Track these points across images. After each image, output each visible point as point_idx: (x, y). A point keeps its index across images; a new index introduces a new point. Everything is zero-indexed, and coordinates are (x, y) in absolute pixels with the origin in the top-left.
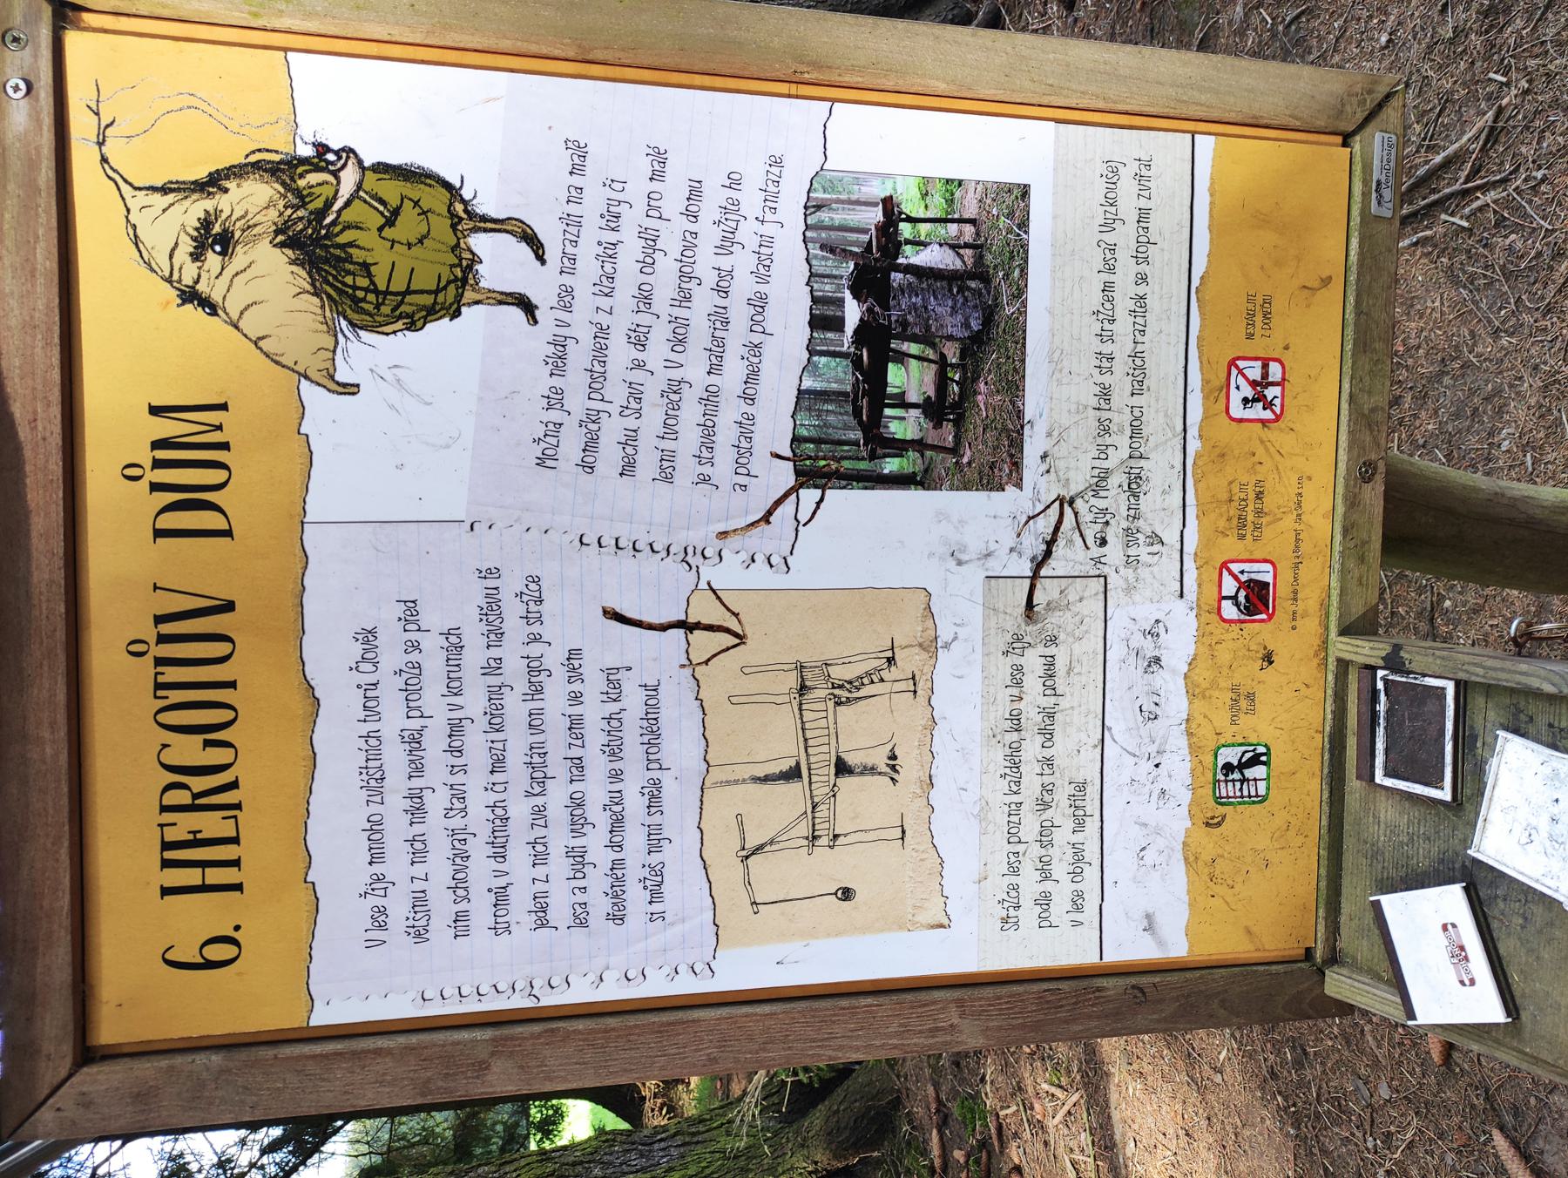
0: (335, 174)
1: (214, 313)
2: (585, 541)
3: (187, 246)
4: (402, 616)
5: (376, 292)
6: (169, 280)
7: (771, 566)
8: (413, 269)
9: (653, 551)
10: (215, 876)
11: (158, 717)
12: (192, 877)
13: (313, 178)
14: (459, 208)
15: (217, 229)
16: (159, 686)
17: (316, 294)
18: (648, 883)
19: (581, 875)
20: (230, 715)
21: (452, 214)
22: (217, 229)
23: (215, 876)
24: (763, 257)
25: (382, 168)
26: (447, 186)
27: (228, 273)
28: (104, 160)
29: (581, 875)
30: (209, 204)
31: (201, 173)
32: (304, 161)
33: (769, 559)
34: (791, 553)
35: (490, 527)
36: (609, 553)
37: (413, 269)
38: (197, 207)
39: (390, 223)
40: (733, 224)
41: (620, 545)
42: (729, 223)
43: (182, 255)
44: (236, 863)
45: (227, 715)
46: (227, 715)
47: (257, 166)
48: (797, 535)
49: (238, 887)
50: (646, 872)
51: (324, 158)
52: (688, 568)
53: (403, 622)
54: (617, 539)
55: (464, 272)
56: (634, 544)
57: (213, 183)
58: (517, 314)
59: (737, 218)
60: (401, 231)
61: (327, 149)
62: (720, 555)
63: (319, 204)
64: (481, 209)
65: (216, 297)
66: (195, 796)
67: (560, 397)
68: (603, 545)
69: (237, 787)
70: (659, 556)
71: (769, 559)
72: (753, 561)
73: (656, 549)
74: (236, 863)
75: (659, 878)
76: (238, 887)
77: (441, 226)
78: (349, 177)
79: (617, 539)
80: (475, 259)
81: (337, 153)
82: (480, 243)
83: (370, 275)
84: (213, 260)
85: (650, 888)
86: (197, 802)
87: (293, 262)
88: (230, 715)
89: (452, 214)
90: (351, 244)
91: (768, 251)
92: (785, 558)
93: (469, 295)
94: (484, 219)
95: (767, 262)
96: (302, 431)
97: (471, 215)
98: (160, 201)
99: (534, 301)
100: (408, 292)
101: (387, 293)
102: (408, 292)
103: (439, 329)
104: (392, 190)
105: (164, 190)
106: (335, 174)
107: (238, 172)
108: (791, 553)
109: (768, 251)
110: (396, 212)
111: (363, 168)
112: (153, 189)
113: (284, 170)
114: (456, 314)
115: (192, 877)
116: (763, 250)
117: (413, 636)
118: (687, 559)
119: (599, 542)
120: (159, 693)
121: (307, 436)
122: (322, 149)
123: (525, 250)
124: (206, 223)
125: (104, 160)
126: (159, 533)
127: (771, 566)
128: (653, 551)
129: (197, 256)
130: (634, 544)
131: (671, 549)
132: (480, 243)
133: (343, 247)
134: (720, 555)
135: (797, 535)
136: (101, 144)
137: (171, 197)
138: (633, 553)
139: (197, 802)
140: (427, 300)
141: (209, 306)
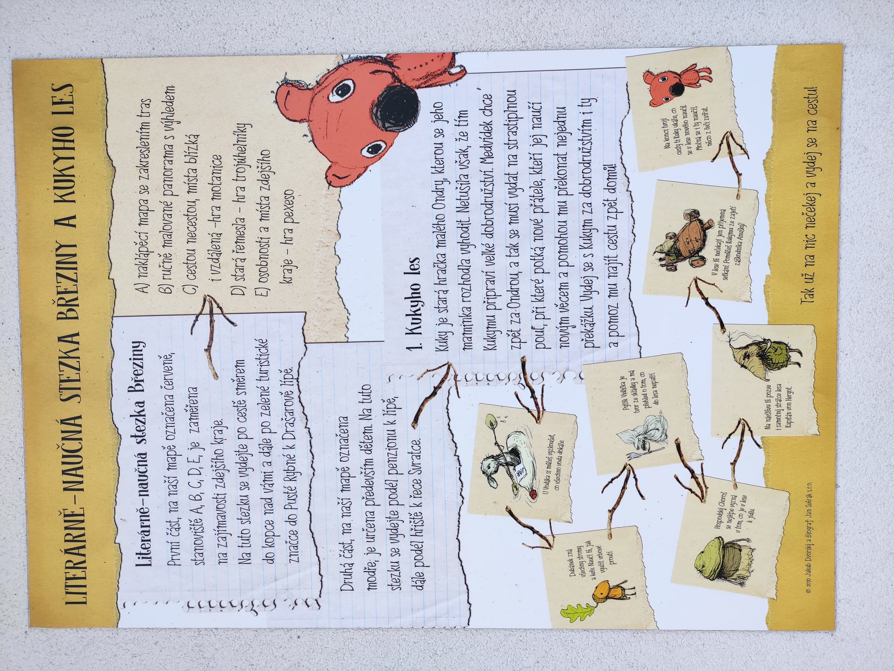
0: (767, 344)
1: (746, 368)
2: (190, 605)
3: (742, 357)
5: (773, 363)
6: (739, 363)
7: (308, 606)
8: (75, 496)
9: (232, 606)
10: (67, 145)
12: (61, 145)
13: (763, 345)
14: (787, 348)
15: (747, 354)
16: (60, 389)
17: (763, 364)
20: (72, 131)
21: (786, 349)
22: (747, 354)
23: (67, 145)
25: (775, 342)
26: (785, 344)
27: (749, 361)
28: (730, 344)
30: (746, 350)
31: (745, 345)
32: (761, 342)
33: (306, 602)
34: (320, 596)
35: (134, 604)
37: (75, 496)
38: (745, 351)
39: (776, 351)
41: (212, 606)
43: (742, 359)
47: (754, 343)
48: (322, 584)
51: (765, 341)
52: (256, 614)
55: (788, 359)
56: (220, 603)
57: (747, 347)
58: (797, 366)
60: (778, 353)
61: (766, 340)
62: (274, 603)
63: (764, 349)
64: (791, 348)
65: (747, 366)
67: (248, 518)
68: (202, 606)
69: (83, 469)
70: (236, 609)
71: (306, 602)
72: (296, 604)
73: (234, 605)
77: (784, 351)
78: (769, 344)
80: (790, 357)
81: (767, 340)
82: (791, 354)
83: (772, 361)
84: (746, 360)
87: (759, 359)
88: (72, 131)
89: (786, 349)
90: (769, 355)
92: (316, 600)
93: (789, 363)
94: (792, 349)
96: (116, 542)
97: (790, 349)
98: (738, 350)
99: (800, 363)
100: (778, 363)
101: (775, 363)
102: (778, 363)
103: (783, 369)
104: (776, 346)
105: (739, 349)
106: (767, 344)
107: (751, 345)
108: (320, 596)
110: (777, 349)
111: (771, 342)
112: (737, 349)
113: (758, 344)
114: (787, 366)
115: (61, 145)
118: (254, 609)
119: (199, 605)
120: (60, 391)
121: (119, 544)
122: (765, 340)
123: (799, 355)
124: (746, 354)
125: (730, 344)
126: (58, 318)
127: (308, 606)
128: (232, 606)
129: (744, 359)
130: (220, 603)
131: (243, 604)
132: (791, 354)
133: (767, 356)
134: (274, 603)
135: (322, 584)
136: (730, 342)
137: (740, 350)
138: (220, 609)
140: (782, 364)
141: (746, 368)
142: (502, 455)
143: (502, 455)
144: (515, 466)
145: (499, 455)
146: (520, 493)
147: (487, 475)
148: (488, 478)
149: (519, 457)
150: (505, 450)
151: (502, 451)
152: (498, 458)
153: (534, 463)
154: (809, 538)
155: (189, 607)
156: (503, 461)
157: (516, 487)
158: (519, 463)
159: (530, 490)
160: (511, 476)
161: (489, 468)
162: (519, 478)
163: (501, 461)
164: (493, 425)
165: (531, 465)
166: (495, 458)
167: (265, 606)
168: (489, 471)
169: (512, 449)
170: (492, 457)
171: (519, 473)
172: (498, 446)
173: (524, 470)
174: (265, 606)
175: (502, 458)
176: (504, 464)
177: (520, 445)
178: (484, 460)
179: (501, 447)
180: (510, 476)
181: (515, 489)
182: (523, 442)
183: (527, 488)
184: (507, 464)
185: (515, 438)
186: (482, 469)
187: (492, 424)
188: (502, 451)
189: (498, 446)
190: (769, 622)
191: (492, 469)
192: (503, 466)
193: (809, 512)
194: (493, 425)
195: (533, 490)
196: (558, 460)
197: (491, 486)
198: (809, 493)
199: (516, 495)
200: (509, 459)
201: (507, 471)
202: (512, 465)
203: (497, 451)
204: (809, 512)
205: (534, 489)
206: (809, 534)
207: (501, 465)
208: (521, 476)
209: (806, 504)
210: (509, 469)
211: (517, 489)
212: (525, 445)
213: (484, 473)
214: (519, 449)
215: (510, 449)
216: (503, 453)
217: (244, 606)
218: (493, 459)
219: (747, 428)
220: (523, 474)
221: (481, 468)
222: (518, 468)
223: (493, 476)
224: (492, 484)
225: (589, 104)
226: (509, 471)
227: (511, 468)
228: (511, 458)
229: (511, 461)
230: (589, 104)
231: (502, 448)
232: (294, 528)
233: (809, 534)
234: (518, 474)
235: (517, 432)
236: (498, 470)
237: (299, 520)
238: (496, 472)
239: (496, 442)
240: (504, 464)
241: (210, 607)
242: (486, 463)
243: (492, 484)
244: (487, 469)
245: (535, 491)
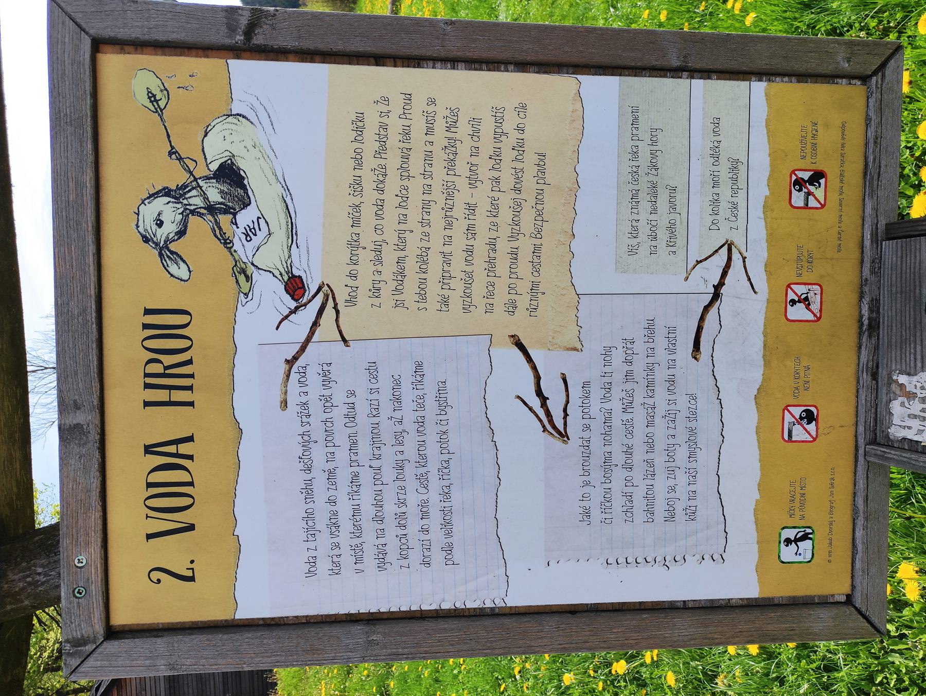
2: (609, 562)
4: (486, 296)
7: (714, 561)
9: (647, 562)
11: (186, 278)
12: (162, 395)
18: (625, 401)
19: (588, 474)
24: (671, 339)
29: (588, 474)
33: (712, 557)
36: (623, 567)
40: (673, 416)
42: (670, 416)
44: (190, 388)
45: (188, 501)
46: (188, 501)
49: (191, 404)
50: (623, 394)
53: (487, 271)
54: (626, 559)
59: (675, 412)
66: (166, 368)
71: (712, 557)
72: (703, 559)
74: (190, 388)
75: (631, 399)
76: (191, 404)
79: (626, 559)
85: (626, 404)
86: (166, 372)
91: (673, 335)
95: (674, 342)
109: (673, 335)
115: (162, 395)
116: (671, 335)
117: (491, 279)
121: (238, 536)
127: (714, 561)
128: (647, 562)
139: (166, 372)
142: (194, 184)
143: (193, 184)
144: (235, 215)
145: (184, 186)
146: (257, 290)
147: (157, 244)
148: (161, 255)
149: (244, 188)
150: (201, 171)
151: (191, 173)
152: (181, 196)
153: (288, 200)
154: (832, 516)
155: (608, 564)
156: (197, 202)
157: (243, 271)
158: (246, 204)
159: (286, 278)
160: (227, 243)
161: (160, 224)
162: (250, 247)
163: (192, 201)
164: (157, 101)
165: (281, 207)
166: (175, 194)
167: (676, 561)
168: (161, 234)
169: (222, 166)
170: (166, 192)
171: (249, 234)
172: (180, 159)
173: (262, 221)
174: (676, 561)
175: (194, 193)
176: (203, 211)
177: (243, 153)
178: (143, 202)
179: (186, 161)
180: (225, 243)
181: (242, 278)
182: (249, 144)
183: (277, 273)
184: (211, 209)
185: (227, 133)
186: (141, 229)
187: (154, 96)
188: (191, 173)
189: (180, 159)
190: (758, 570)
191: (170, 228)
192: (201, 215)
193: (832, 494)
194: (157, 101)
195: (294, 276)
196: (375, 208)
197: (172, 275)
198: (832, 477)
199: (246, 295)
200: (214, 196)
201: (214, 231)
202: (226, 211)
203: (176, 177)
204: (832, 494)
205: (296, 272)
206: (831, 512)
207: (193, 212)
208: (256, 241)
209: (830, 486)
210: (217, 223)
211: (248, 278)
212: (255, 153)
213: (146, 240)
214: (241, 163)
215: (214, 167)
216: (196, 179)
217: (657, 562)
218: (168, 199)
219: (330, 303)
220: (261, 235)
221: (137, 226)
222: (245, 217)
223: (172, 247)
224: (173, 269)
225: (673, 448)
226: (220, 229)
227: (224, 219)
228: (221, 192)
229: (221, 200)
230: (673, 448)
231: (191, 165)
232: (334, 508)
233: (831, 512)
234: (247, 235)
235: (229, 116)
236: (186, 227)
237: (338, 501)
238: (181, 233)
239: (172, 148)
240: (203, 211)
241: (627, 563)
242: (149, 212)
243: (173, 269)
244: (154, 227)
245: (300, 277)
